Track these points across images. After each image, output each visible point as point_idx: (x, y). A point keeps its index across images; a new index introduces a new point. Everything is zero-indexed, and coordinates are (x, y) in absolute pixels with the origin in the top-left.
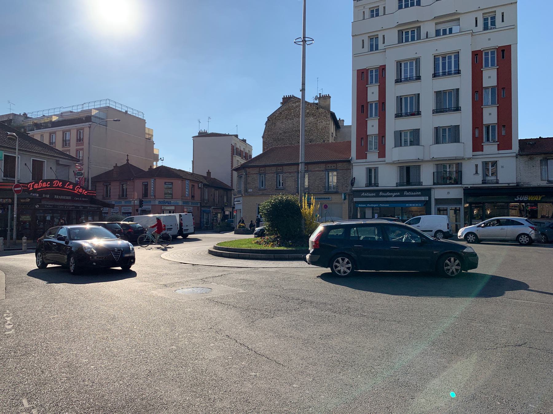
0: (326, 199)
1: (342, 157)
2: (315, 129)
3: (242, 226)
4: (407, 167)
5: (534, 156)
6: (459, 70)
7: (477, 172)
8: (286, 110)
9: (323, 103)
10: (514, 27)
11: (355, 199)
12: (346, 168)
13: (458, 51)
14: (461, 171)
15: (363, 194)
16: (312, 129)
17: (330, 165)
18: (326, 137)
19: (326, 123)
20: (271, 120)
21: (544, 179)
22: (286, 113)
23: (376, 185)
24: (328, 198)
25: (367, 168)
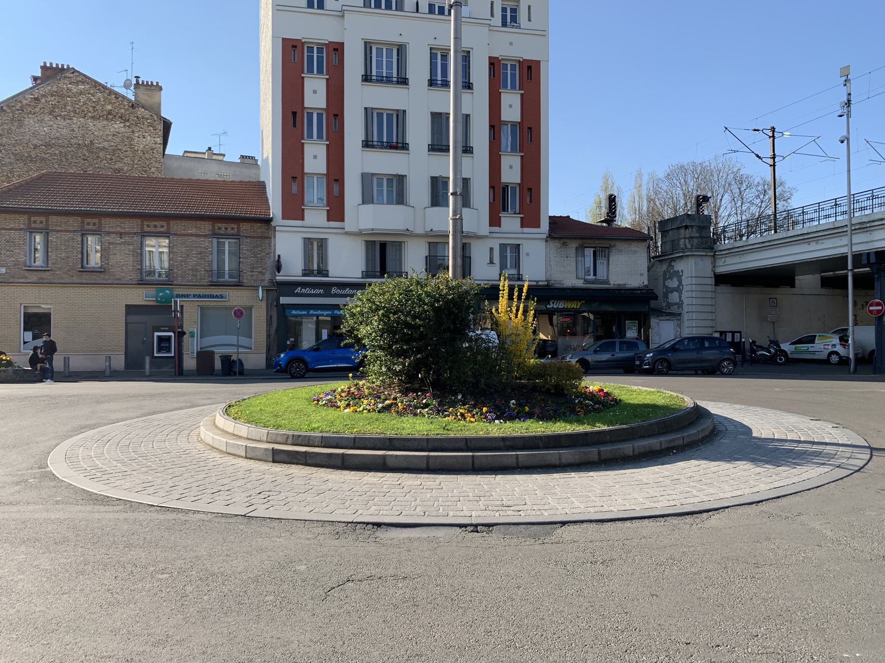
0: (217, 297)
1: (254, 211)
2: (129, 149)
3: (6, 360)
4: (380, 244)
5: (568, 241)
6: (469, 83)
7: (491, 262)
8: (52, 95)
9: (144, 97)
10: (543, 34)
11: (284, 300)
12: (260, 235)
13: (469, 50)
14: (470, 257)
15: (298, 290)
16: (120, 147)
17: (223, 226)
18: (153, 169)
19: (154, 141)
20: (9, 111)
21: (580, 277)
22: (50, 103)
23: (323, 272)
24: (221, 296)
25: (304, 238)
